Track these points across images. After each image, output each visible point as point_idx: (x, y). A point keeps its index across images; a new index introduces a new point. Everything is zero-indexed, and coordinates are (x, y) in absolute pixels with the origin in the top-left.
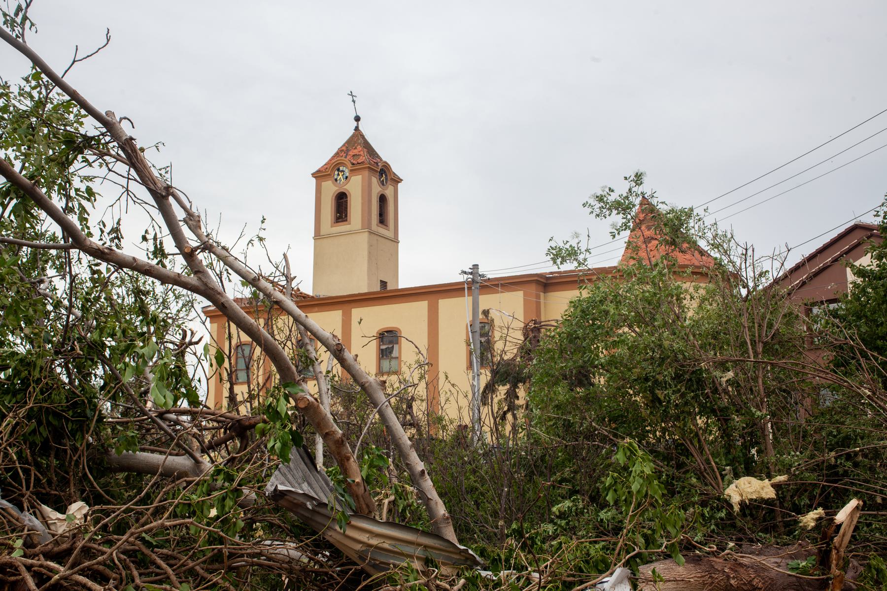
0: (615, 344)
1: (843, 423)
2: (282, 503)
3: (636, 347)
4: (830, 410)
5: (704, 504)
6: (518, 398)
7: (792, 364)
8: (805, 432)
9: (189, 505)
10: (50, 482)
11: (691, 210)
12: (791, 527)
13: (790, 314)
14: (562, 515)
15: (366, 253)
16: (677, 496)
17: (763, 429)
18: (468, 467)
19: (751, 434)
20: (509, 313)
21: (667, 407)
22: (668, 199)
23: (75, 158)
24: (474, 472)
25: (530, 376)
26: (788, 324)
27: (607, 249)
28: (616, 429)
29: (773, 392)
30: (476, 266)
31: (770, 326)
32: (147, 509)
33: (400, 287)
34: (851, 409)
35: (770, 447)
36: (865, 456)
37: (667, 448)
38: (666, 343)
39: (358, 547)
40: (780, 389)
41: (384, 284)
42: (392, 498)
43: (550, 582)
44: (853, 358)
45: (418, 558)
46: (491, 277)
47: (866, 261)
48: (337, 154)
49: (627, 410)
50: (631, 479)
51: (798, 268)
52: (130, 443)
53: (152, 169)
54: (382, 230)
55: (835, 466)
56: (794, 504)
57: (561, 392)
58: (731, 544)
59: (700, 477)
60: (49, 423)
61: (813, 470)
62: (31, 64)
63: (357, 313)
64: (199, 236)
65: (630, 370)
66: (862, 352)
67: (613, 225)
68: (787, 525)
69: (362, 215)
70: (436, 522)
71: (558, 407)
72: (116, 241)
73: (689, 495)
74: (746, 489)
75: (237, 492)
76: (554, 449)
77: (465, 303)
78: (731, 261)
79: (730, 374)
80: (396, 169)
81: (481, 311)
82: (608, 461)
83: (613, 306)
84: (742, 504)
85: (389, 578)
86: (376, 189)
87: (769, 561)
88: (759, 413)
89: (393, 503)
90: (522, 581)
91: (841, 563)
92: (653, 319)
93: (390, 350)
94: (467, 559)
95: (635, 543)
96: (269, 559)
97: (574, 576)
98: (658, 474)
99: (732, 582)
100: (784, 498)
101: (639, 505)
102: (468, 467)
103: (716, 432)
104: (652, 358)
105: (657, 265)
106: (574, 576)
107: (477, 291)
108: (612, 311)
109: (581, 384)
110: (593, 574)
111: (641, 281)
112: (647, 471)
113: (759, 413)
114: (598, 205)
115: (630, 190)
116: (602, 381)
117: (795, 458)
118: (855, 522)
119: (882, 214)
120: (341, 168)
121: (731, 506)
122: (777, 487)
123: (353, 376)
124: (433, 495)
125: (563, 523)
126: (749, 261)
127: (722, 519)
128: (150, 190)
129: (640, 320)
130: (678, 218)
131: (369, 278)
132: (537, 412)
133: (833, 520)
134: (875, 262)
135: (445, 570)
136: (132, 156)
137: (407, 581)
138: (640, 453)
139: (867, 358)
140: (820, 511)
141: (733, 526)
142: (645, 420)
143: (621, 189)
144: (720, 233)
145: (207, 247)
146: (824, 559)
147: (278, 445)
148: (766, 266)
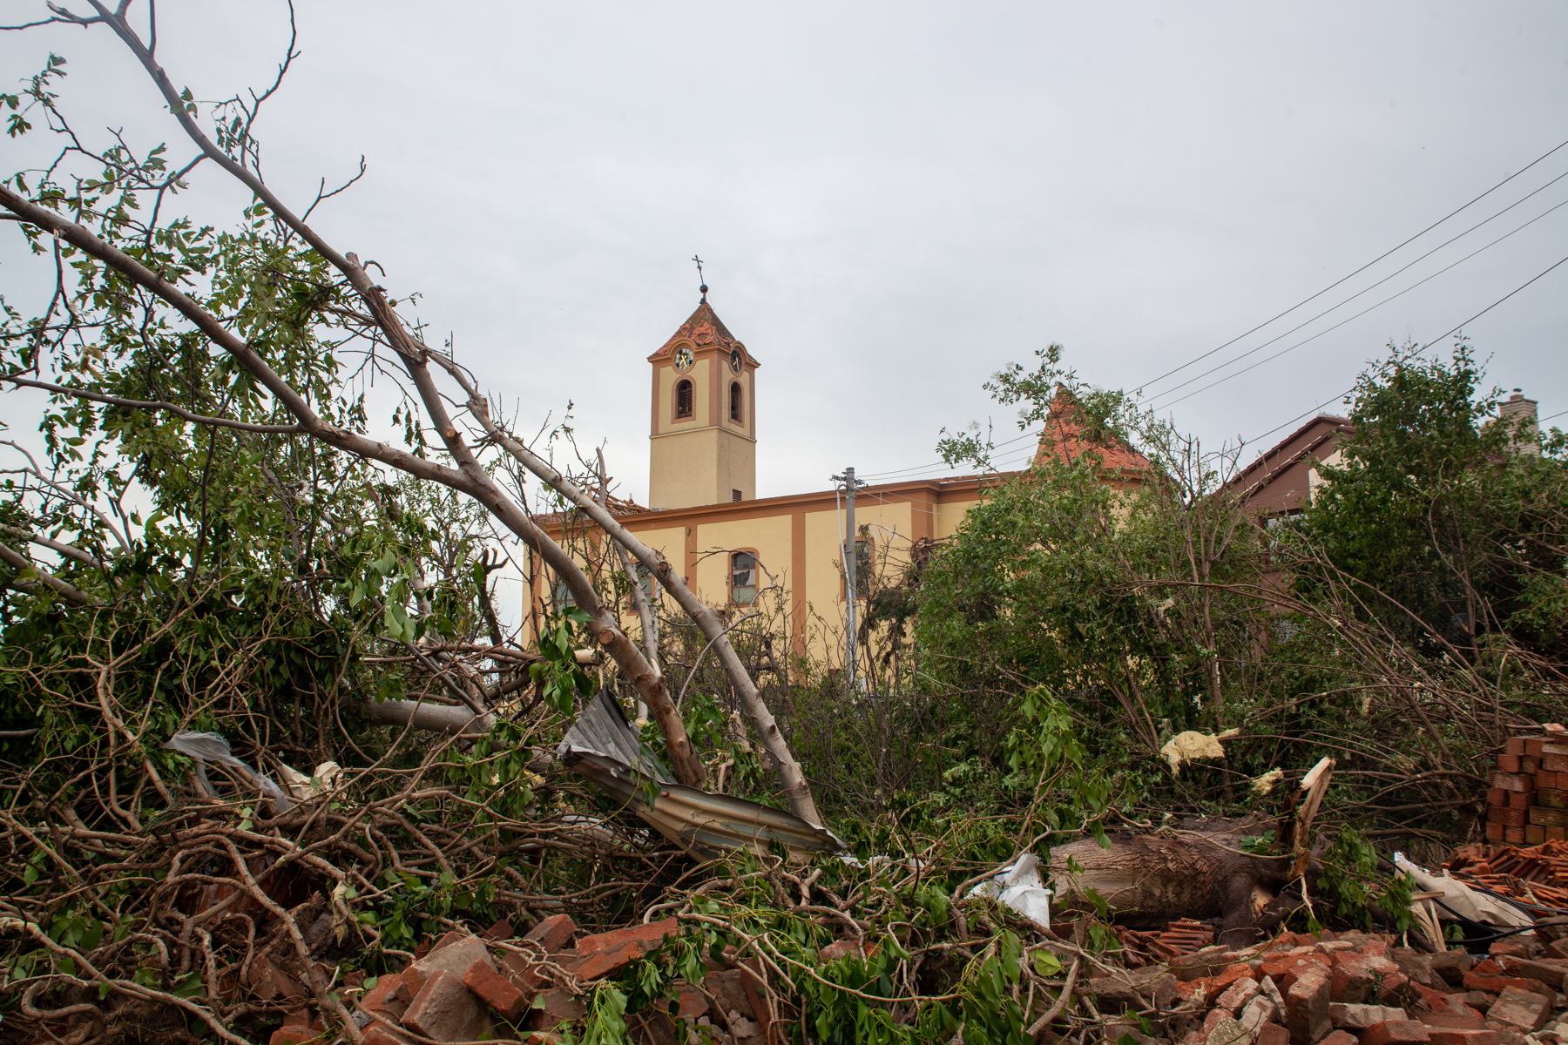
0: (1025, 565)
1: (1306, 662)
2: (579, 768)
3: (1052, 568)
4: (1291, 646)
5: (1133, 766)
6: (904, 635)
7: (1246, 588)
8: (1261, 674)
9: (463, 769)
10: (294, 737)
11: (1121, 393)
12: (1241, 792)
13: (1244, 525)
14: (956, 782)
15: (715, 456)
16: (1102, 756)
17: (1210, 671)
18: (838, 722)
19: (1195, 678)
20: (894, 531)
21: (1090, 644)
22: (1090, 376)
23: (309, 315)
24: (846, 727)
25: (915, 608)
26: (1241, 538)
27: (1014, 446)
28: (1026, 673)
29: (1223, 624)
30: (850, 470)
31: (1219, 540)
32: (411, 775)
33: (758, 496)
34: (1316, 644)
35: (1218, 693)
36: (1332, 702)
37: (1090, 696)
38: (1089, 563)
39: (680, 827)
40: (1231, 620)
41: (737, 494)
42: (731, 762)
43: (933, 873)
44: (1320, 581)
45: (759, 841)
46: (871, 484)
47: (1336, 460)
48: (679, 333)
49: (1039, 648)
50: (1042, 738)
51: (1252, 469)
52: (393, 689)
53: (406, 328)
54: (735, 428)
55: (1297, 715)
56: (1246, 764)
57: (956, 625)
58: (1168, 815)
59: (1133, 735)
60: (290, 662)
61: (1270, 721)
62: (251, 193)
64: (485, 425)
65: (1043, 597)
66: (1331, 572)
67: (1022, 413)
68: (1236, 789)
70: (789, 792)
71: (952, 645)
72: (358, 423)
73: (1116, 755)
74: (1188, 746)
75: (525, 753)
76: (947, 699)
77: (838, 516)
78: (1170, 459)
79: (1170, 602)
80: (752, 350)
81: (857, 527)
82: (1014, 714)
83: (1022, 515)
84: (1182, 764)
85: (719, 868)
86: (728, 376)
87: (1217, 838)
88: (1205, 651)
89: (733, 768)
90: (897, 871)
91: (1306, 838)
92: (1073, 532)
93: (746, 577)
94: (825, 842)
95: (1046, 822)
96: (562, 839)
97: (965, 864)
98: (1077, 730)
99: (1170, 865)
100: (1233, 757)
101: (1052, 771)
102: (838, 722)
103: (1150, 676)
104: (1072, 582)
105: (1077, 463)
106: (965, 864)
107: (852, 501)
108: (1021, 522)
109: (983, 618)
110: (991, 862)
111: (1058, 486)
112: (1064, 727)
113: (1205, 651)
114: (1003, 387)
115: (1043, 368)
116: (1009, 613)
117: (1248, 706)
118: (1325, 787)
119: (1353, 400)
121: (1168, 768)
122: (1225, 743)
123: (682, 604)
124: (786, 757)
125: (958, 791)
126: (1193, 458)
127: (1156, 784)
128: (401, 355)
129: (1056, 534)
130: (1105, 404)
131: (719, 487)
132: (926, 652)
133: (1298, 784)
134: (1346, 461)
135: (794, 857)
136: (380, 315)
137: (742, 872)
138: (1054, 702)
139: (1337, 581)
140: (1278, 771)
141: (1171, 792)
142: (1062, 662)
143: (1032, 366)
144: (1156, 422)
145: (494, 437)
146: (1285, 834)
147: (557, 692)
148: (1215, 465)
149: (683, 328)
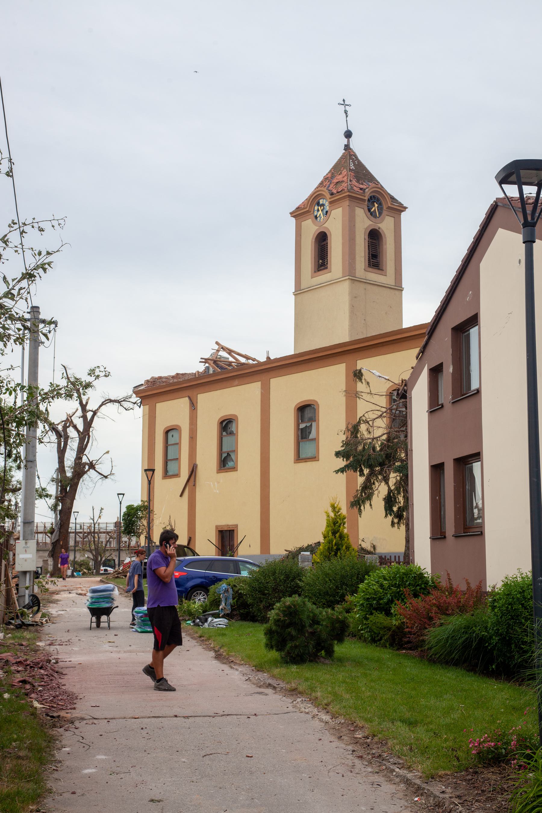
54: (374, 276)
63: (278, 384)
69: (343, 255)
86: (363, 222)
120: (321, 202)
149: (326, 178)
